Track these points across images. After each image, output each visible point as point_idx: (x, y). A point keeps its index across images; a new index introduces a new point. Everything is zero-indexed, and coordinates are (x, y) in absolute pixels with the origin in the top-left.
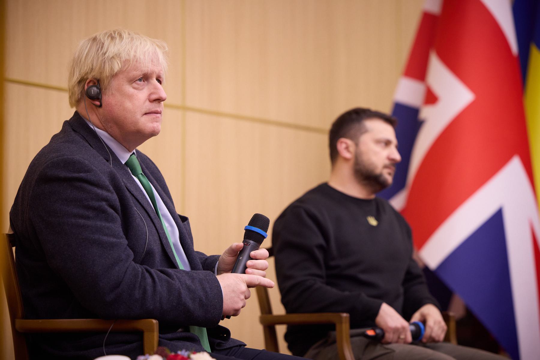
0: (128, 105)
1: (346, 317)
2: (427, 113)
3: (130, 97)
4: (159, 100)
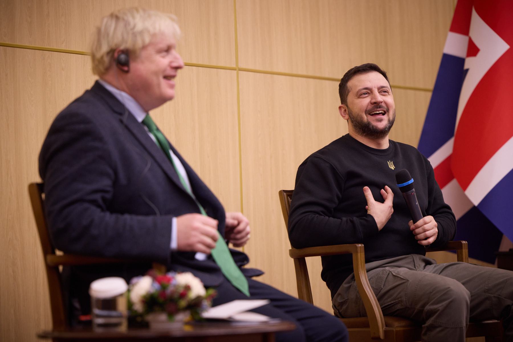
1: (360, 247)
2: (470, 63)
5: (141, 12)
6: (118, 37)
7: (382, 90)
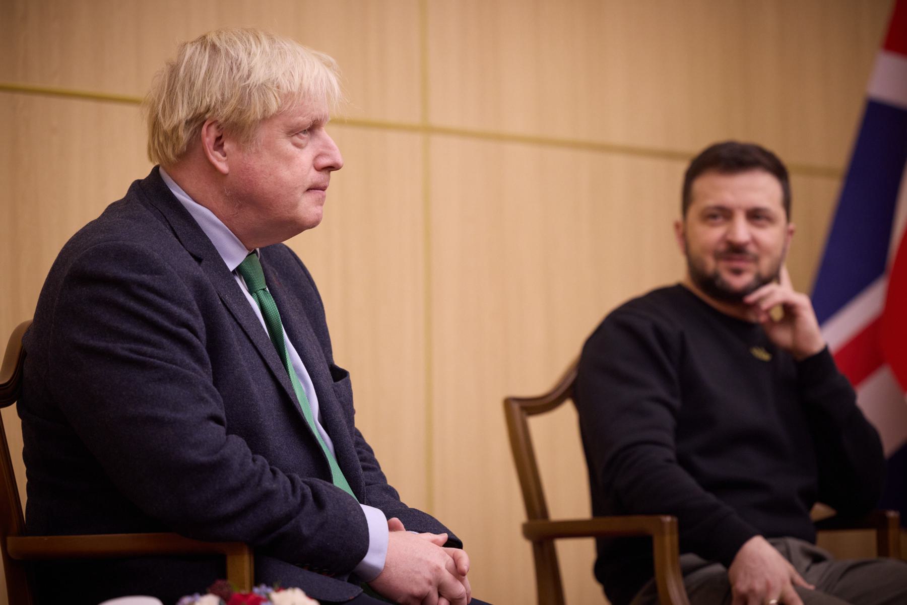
0: (285, 174)
1: (671, 523)
3: (288, 160)
5: (265, 42)
7: (755, 215)
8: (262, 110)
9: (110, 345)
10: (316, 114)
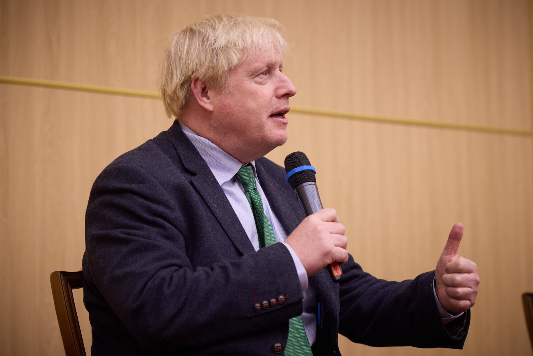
0: (251, 104)
3: (253, 94)
4: (288, 95)
6: (194, 58)
8: (227, 64)
9: (109, 231)
10: (267, 60)
